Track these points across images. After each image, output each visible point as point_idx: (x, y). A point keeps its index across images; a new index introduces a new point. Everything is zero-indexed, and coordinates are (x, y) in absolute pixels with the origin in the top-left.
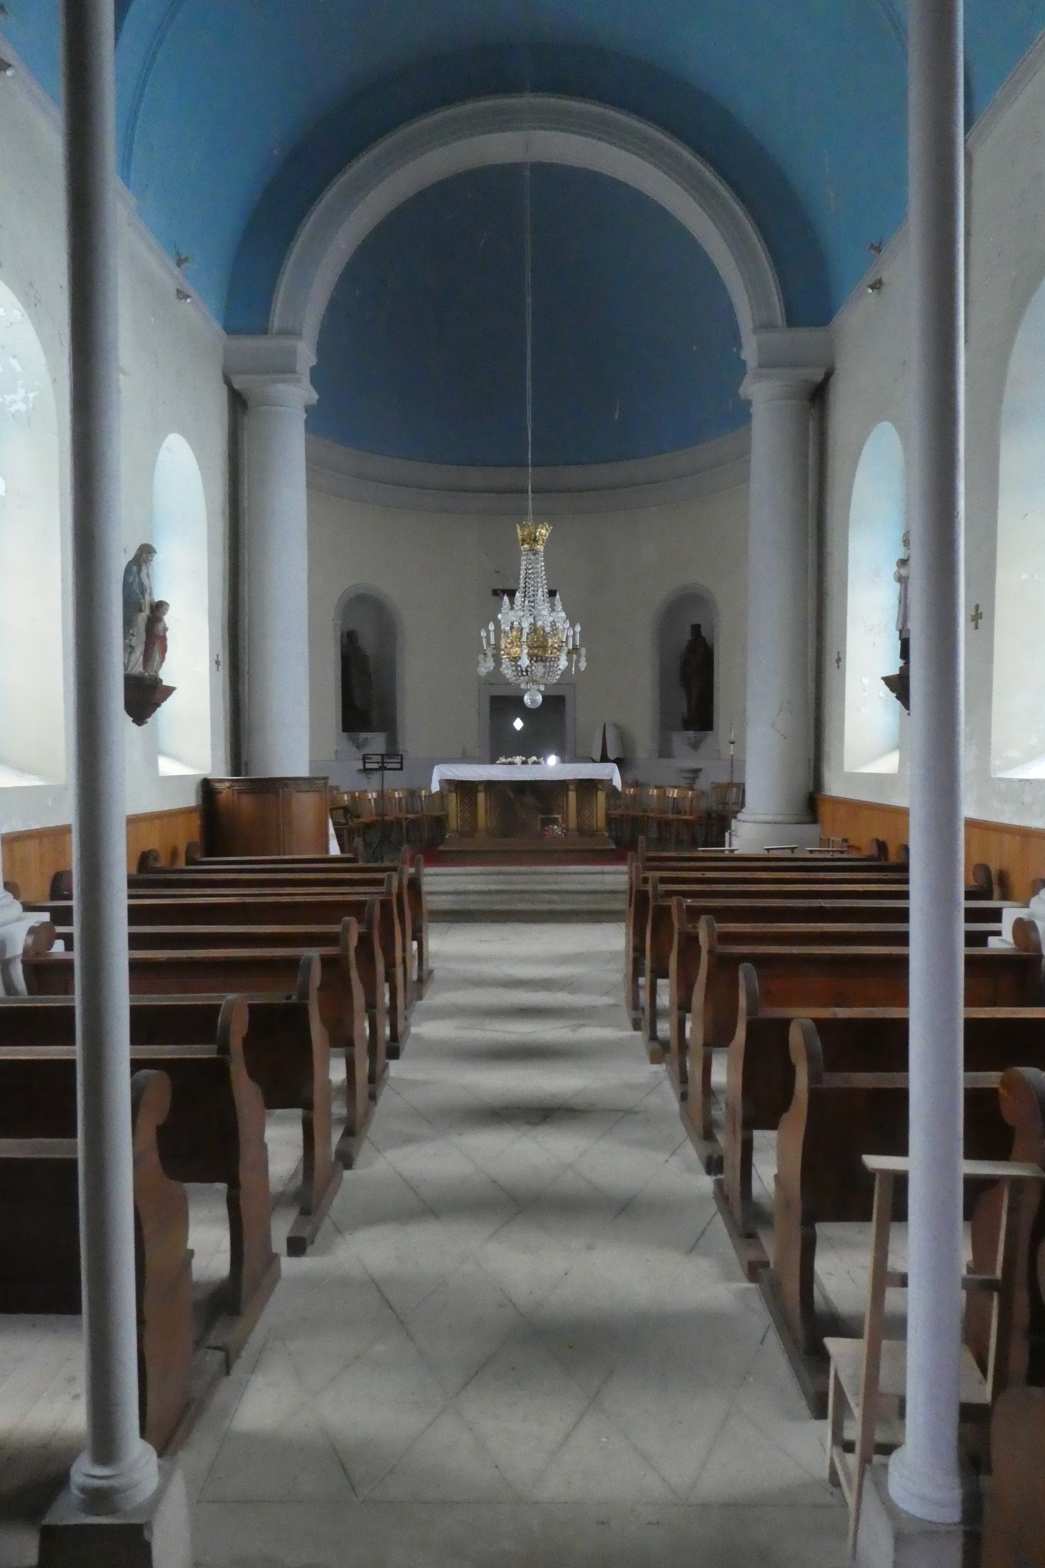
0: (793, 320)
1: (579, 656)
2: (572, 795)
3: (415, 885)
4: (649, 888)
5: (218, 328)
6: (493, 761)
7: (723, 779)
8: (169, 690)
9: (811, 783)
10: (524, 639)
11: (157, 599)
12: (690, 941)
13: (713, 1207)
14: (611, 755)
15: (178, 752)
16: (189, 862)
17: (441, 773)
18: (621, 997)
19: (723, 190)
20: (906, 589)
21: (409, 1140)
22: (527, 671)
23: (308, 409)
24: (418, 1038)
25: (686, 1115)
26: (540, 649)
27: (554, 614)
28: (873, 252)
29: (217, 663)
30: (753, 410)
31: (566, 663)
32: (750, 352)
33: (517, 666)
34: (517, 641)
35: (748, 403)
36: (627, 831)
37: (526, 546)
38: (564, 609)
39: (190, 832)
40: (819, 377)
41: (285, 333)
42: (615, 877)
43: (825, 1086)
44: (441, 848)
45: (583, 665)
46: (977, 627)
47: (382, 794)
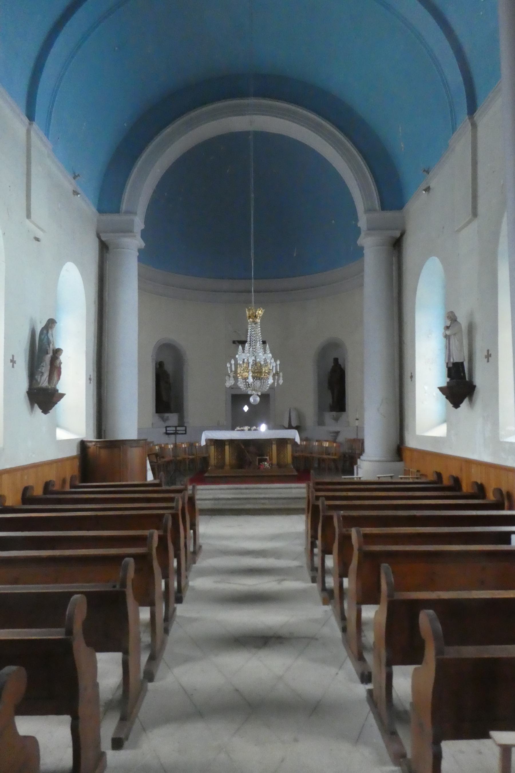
0: (384, 207)
1: (279, 376)
2: (274, 447)
3: (192, 500)
4: (320, 503)
5: (94, 210)
6: (233, 429)
7: (353, 436)
8: (62, 395)
9: (399, 441)
10: (250, 368)
11: (57, 347)
12: (346, 539)
13: (367, 708)
14: (294, 424)
15: (72, 423)
16: (72, 487)
17: (206, 436)
18: (303, 561)
19: (348, 144)
20: (449, 341)
21: (187, 660)
22: (251, 385)
23: (139, 251)
24: (193, 589)
25: (346, 642)
26: (258, 373)
27: (265, 355)
28: (425, 173)
29: (90, 379)
30: (364, 252)
31: (272, 381)
32: (363, 222)
33: (246, 382)
34: (246, 369)
35: (362, 248)
36: (303, 466)
37: (251, 320)
38: (271, 352)
39: (72, 471)
40: (397, 234)
41: (128, 212)
42: (299, 490)
43: (446, 656)
44: (206, 475)
45: (281, 382)
46: (488, 361)
47: (175, 445)
